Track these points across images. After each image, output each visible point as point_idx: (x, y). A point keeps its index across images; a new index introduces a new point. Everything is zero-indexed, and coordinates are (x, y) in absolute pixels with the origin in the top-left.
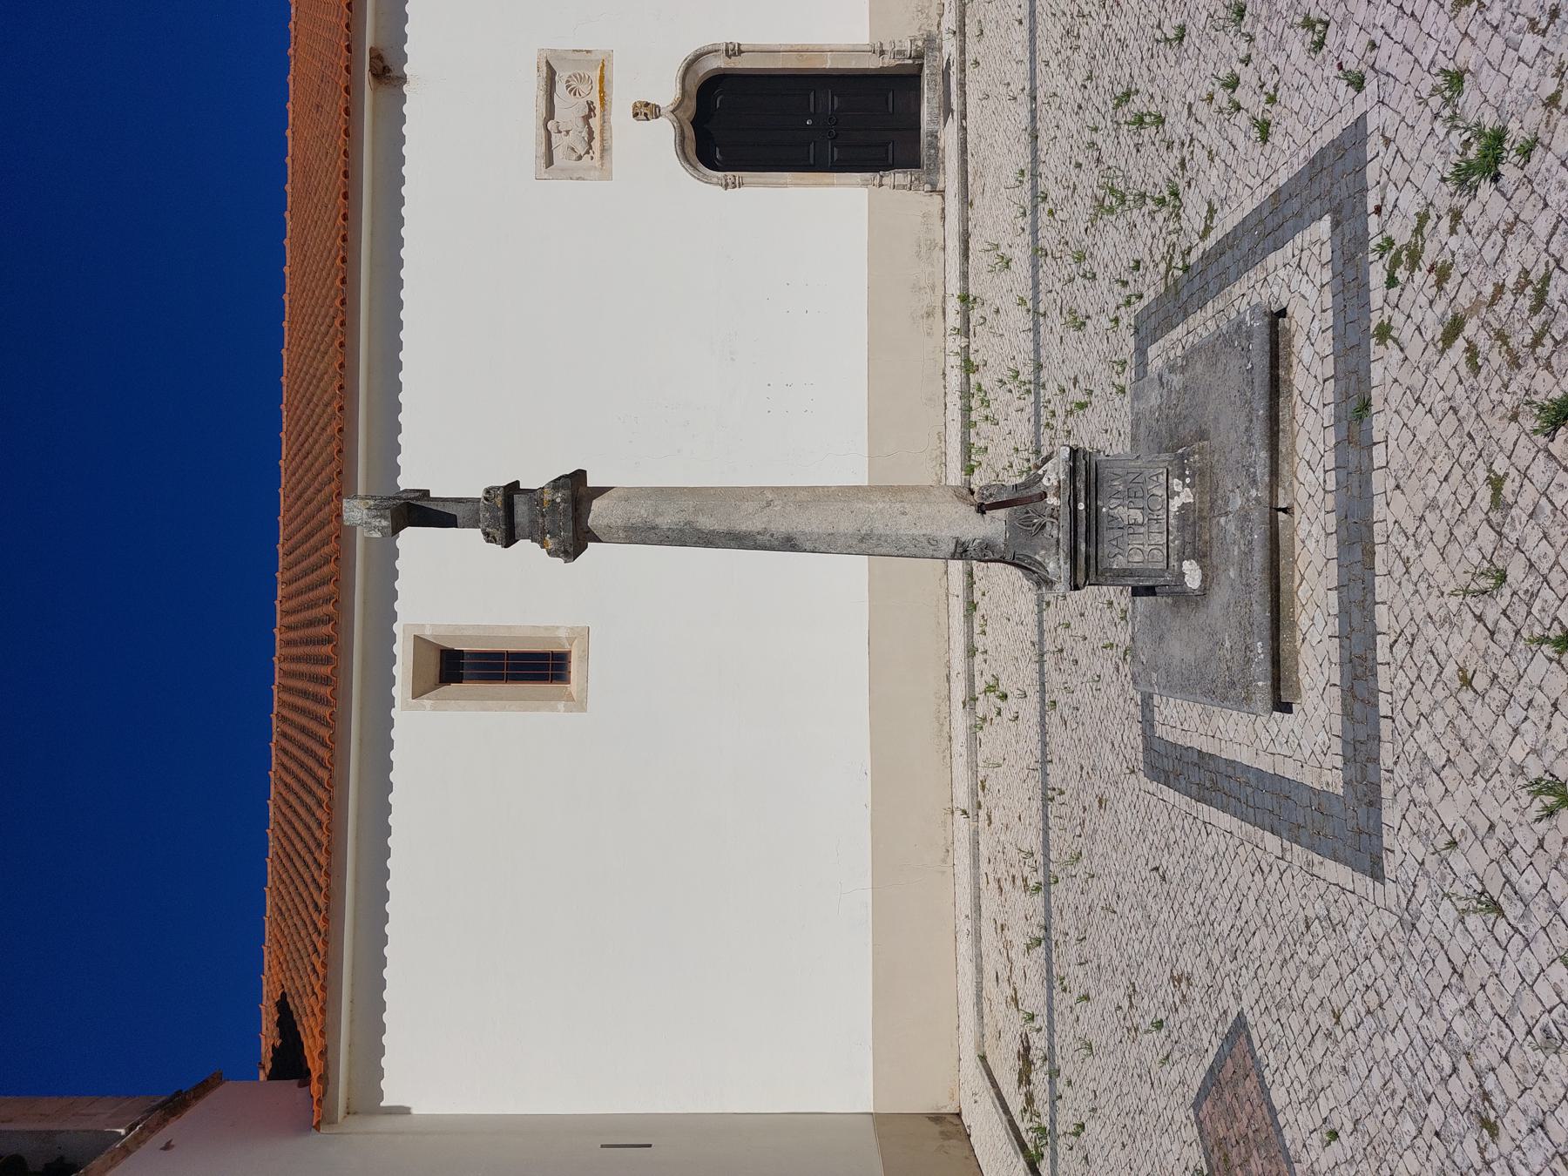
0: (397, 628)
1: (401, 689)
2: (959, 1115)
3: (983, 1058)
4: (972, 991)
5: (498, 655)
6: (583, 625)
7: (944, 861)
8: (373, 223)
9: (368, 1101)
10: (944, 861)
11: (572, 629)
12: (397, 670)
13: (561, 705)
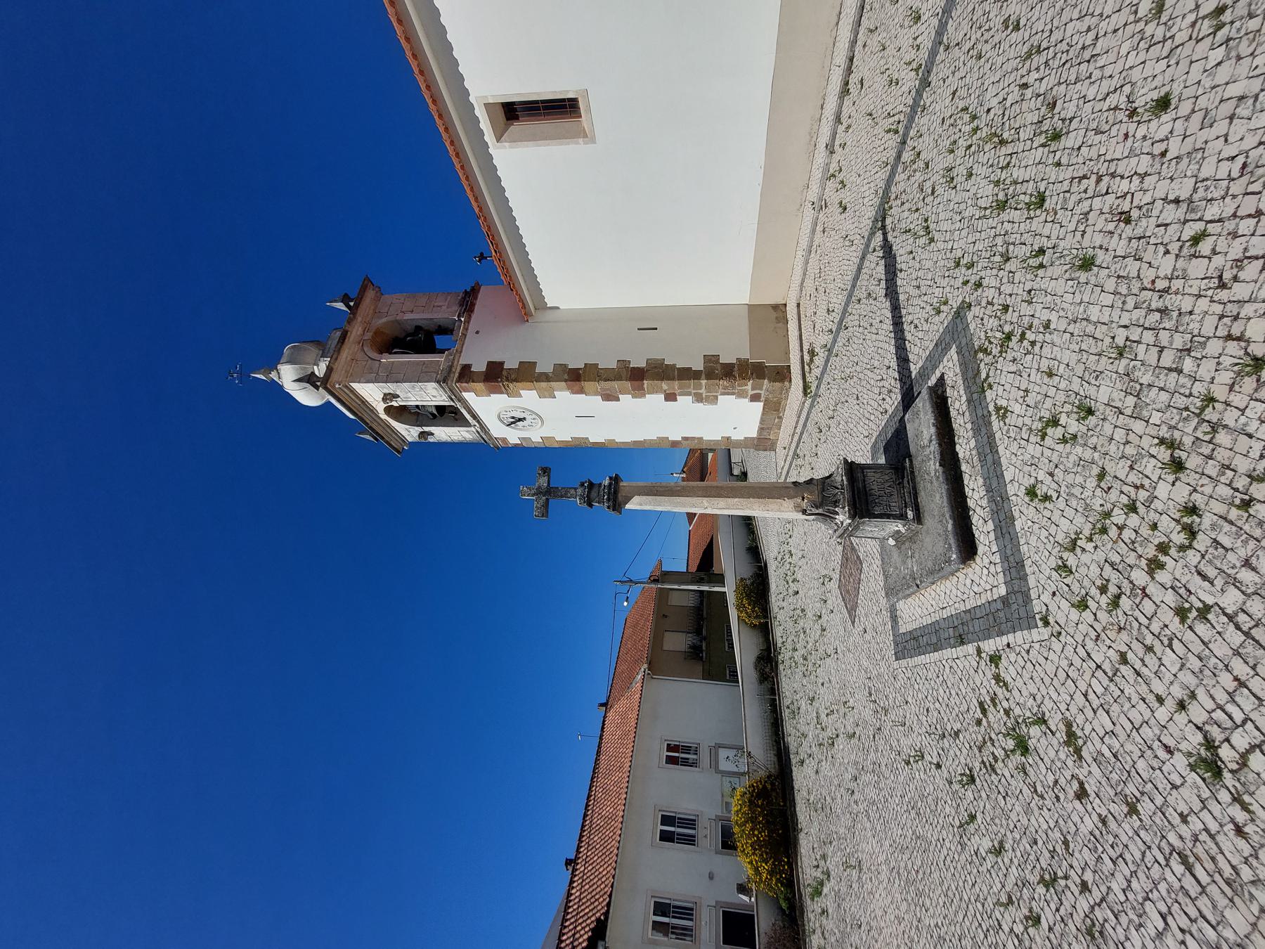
0: (472, 99)
1: (489, 137)
2: (785, 305)
3: (798, 305)
4: (798, 282)
5: (536, 102)
6: (583, 88)
7: (799, 210)
8: (439, 64)
9: (542, 306)
10: (799, 210)
11: (577, 92)
12: (482, 126)
13: (581, 140)
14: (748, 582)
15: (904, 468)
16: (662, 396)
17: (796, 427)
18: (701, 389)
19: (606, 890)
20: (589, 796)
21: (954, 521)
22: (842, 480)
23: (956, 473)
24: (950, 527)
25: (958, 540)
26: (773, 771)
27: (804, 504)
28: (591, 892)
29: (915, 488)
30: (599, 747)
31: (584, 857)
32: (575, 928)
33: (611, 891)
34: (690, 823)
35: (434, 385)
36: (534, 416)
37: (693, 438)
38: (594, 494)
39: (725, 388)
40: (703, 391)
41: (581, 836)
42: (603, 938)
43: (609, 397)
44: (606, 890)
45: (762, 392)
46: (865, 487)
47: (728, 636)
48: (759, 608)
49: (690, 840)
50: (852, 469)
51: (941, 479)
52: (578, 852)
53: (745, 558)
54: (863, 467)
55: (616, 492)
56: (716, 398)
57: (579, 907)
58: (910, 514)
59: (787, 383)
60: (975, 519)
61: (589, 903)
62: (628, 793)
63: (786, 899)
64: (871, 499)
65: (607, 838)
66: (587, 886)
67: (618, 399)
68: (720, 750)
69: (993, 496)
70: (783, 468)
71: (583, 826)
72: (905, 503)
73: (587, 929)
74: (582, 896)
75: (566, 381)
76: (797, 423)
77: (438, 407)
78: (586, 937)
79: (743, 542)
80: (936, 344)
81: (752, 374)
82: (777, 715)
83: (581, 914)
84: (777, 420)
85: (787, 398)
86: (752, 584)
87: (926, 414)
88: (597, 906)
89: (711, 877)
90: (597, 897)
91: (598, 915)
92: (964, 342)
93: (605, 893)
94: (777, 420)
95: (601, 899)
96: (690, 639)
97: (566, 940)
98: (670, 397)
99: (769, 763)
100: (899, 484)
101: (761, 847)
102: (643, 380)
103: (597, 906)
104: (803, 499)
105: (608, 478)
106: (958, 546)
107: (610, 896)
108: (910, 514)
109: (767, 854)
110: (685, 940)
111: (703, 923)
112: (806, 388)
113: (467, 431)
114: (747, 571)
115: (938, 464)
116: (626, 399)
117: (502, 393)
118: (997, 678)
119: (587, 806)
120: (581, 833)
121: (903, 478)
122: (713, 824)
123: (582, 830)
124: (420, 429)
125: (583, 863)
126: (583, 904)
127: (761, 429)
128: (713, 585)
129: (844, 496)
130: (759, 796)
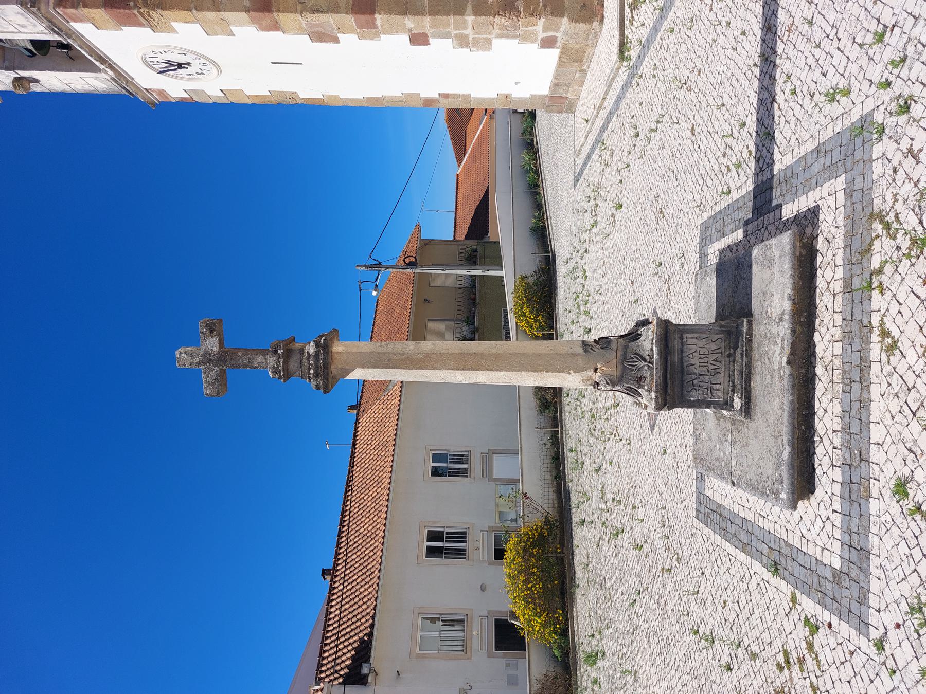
14: (531, 280)
15: (740, 333)
16: (406, 38)
17: (604, 99)
18: (466, 28)
19: (368, 611)
20: (344, 511)
21: (793, 448)
22: (652, 349)
23: (807, 371)
24: (786, 455)
25: (793, 477)
26: (550, 510)
27: (597, 377)
28: (352, 612)
29: (749, 366)
30: (353, 453)
31: (342, 575)
32: (337, 646)
33: (375, 613)
34: (461, 537)
35: (16, 8)
36: (203, 61)
37: (456, 96)
38: (293, 364)
39: (504, 28)
40: (469, 31)
41: (337, 554)
42: (367, 659)
43: (320, 37)
44: (368, 611)
45: (559, 35)
46: (681, 360)
47: (505, 324)
48: (543, 316)
49: (460, 553)
50: (667, 330)
51: (785, 383)
52: (337, 558)
53: (528, 244)
54: (683, 330)
55: (326, 366)
56: (489, 42)
57: (339, 625)
58: (737, 403)
59: (596, 25)
60: (819, 451)
61: (350, 622)
62: (389, 513)
63: (560, 647)
64: (687, 378)
65: (367, 557)
66: (347, 606)
67: (336, 40)
68: (495, 456)
69: (848, 442)
70: (582, 145)
71: (339, 543)
72: (734, 386)
73: (350, 648)
74: (342, 615)
75: (247, 10)
76: (607, 93)
77: (33, 42)
78: (349, 655)
79: (527, 220)
80: (818, 150)
81: (545, 6)
82: (558, 449)
83: (343, 633)
84: (578, 75)
85: (595, 45)
86: (535, 284)
87: (782, 272)
88: (360, 626)
89: (483, 588)
90: (359, 617)
91: (361, 635)
92: (858, 184)
93: (368, 614)
94: (578, 75)
95: (364, 620)
96: (458, 331)
97: (327, 657)
98: (419, 39)
99: (547, 502)
100: (729, 356)
101: (534, 599)
102: (373, 12)
103: (360, 626)
104: (596, 370)
105: (312, 344)
106: (792, 484)
107: (373, 618)
108: (737, 403)
109: (540, 605)
110: (453, 626)
111: (474, 633)
112: (623, 46)
113: (96, 78)
114: (530, 265)
115: (785, 359)
116: (349, 40)
117: (140, 25)
118: (810, 646)
119: (342, 521)
120: (336, 551)
121: (736, 348)
122: (486, 536)
123: (338, 547)
124: (12, 75)
125: (342, 581)
126: (344, 623)
127: (555, 86)
128: (487, 268)
129: (652, 375)
130: (534, 545)
